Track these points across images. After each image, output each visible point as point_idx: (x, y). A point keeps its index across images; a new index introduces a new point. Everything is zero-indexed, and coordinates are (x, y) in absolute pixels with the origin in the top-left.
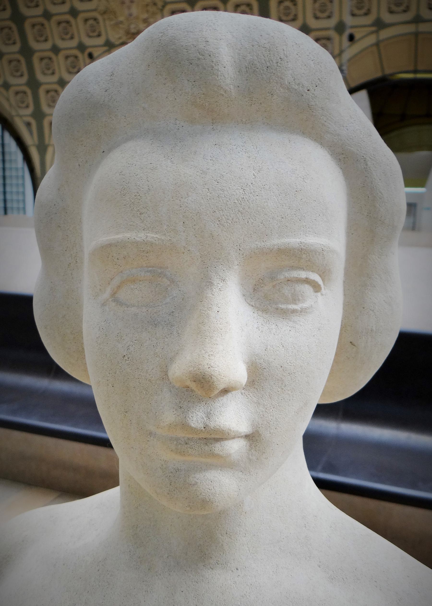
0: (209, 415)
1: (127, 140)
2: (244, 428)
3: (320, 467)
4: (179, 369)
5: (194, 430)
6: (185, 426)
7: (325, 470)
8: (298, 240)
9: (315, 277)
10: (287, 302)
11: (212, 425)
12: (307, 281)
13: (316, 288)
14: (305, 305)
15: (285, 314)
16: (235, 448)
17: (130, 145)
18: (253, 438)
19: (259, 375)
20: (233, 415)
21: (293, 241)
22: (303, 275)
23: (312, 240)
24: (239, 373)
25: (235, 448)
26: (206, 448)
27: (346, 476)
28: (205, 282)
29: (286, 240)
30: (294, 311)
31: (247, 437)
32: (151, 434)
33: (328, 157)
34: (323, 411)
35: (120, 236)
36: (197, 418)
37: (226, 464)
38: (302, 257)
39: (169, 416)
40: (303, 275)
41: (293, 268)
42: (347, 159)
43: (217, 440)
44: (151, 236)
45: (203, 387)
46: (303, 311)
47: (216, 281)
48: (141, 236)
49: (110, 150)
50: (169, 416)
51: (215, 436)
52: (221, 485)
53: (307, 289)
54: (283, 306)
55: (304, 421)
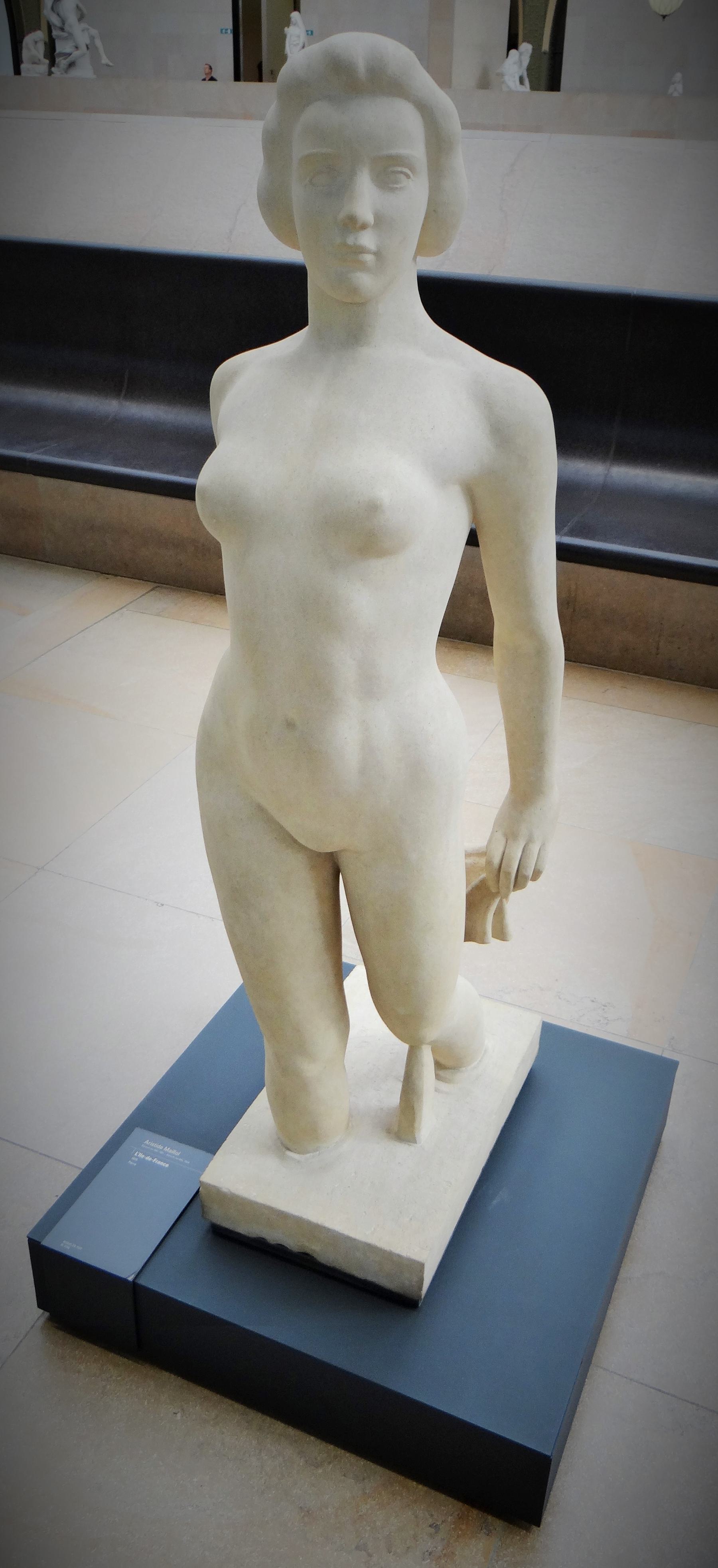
0: (356, 239)
3: (566, 529)
4: (342, 215)
6: (345, 244)
7: (571, 533)
12: (401, 172)
13: (408, 176)
15: (392, 190)
18: (378, 254)
19: (380, 219)
21: (394, 152)
22: (399, 169)
23: (403, 151)
24: (370, 218)
25: (369, 258)
27: (605, 541)
28: (353, 174)
36: (350, 241)
37: (363, 267)
38: (398, 160)
40: (399, 169)
43: (361, 253)
45: (352, 224)
51: (360, 250)
52: (365, 281)
53: (402, 177)
54: (391, 186)
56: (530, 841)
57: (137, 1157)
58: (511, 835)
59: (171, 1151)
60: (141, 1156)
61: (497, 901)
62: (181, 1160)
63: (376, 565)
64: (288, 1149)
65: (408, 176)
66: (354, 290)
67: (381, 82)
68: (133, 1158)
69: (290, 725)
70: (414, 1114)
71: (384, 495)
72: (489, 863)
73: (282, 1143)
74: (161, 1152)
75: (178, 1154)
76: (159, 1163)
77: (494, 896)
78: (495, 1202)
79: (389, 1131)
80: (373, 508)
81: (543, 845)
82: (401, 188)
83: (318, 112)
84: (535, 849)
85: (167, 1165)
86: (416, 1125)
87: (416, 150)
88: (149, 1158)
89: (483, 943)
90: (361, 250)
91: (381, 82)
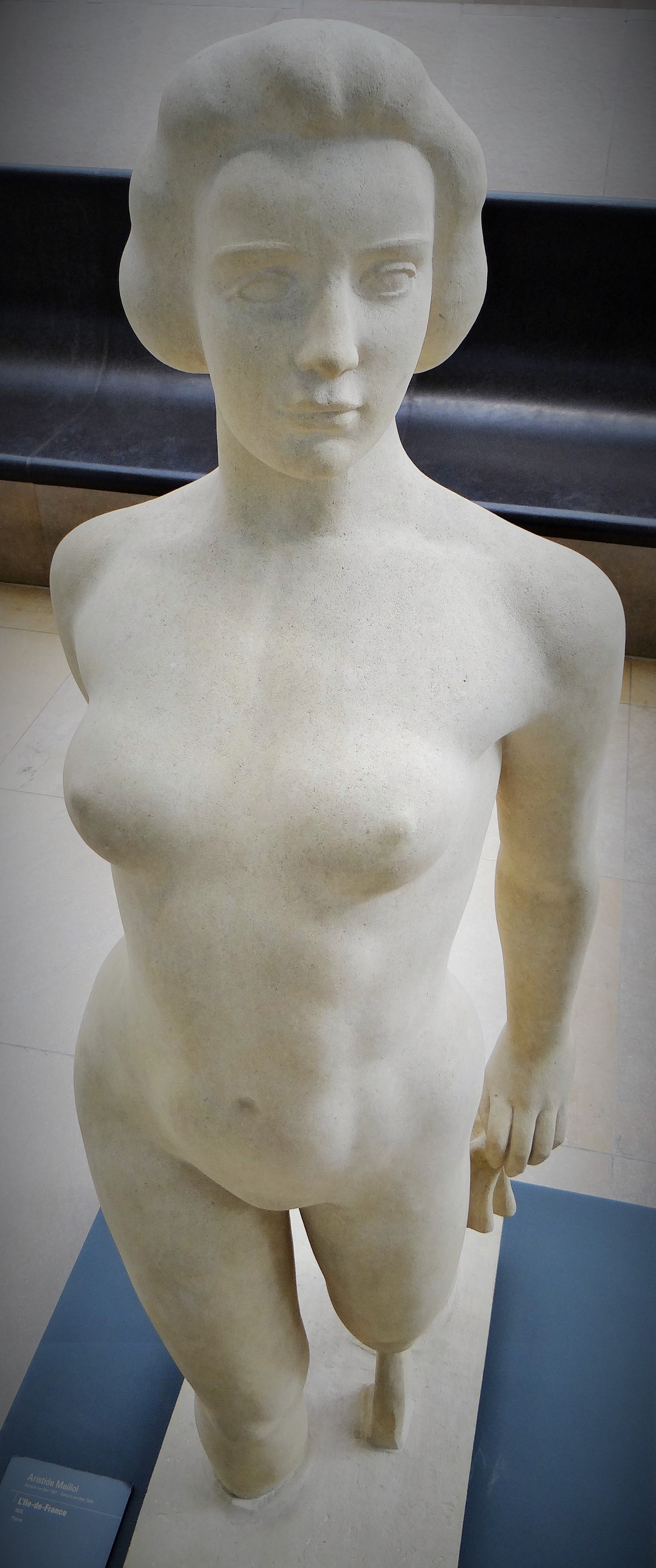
0: (331, 393)
1: (246, 149)
2: (357, 402)
4: (308, 355)
5: (320, 406)
6: (313, 403)
8: (397, 239)
9: (410, 266)
10: (388, 290)
11: (334, 400)
12: (404, 271)
13: (411, 274)
14: (402, 291)
15: (385, 300)
16: (350, 418)
17: (249, 155)
18: (363, 410)
19: (368, 356)
20: (348, 391)
21: (392, 240)
22: (400, 266)
23: (408, 237)
26: (329, 421)
28: (322, 282)
29: (387, 240)
30: (393, 297)
31: (358, 409)
32: (279, 412)
33: (419, 153)
34: (423, 382)
35: (251, 244)
36: (321, 396)
37: (341, 433)
39: (298, 396)
40: (400, 266)
41: (392, 261)
43: (337, 413)
44: (279, 244)
45: (330, 369)
46: (401, 296)
47: (332, 279)
48: (270, 244)
49: (229, 157)
50: (298, 396)
52: (337, 450)
53: (404, 276)
54: (384, 294)
55: (395, 395)
56: (545, 1108)
57: (21, 1507)
58: (518, 1103)
59: (65, 1487)
60: (27, 1503)
61: (497, 1176)
62: (81, 1499)
63: (386, 901)
64: (234, 1496)
65: (411, 274)
66: (325, 469)
67: (374, 115)
68: (18, 1511)
69: (245, 1106)
70: (393, 1420)
71: (407, 814)
72: (495, 1146)
73: (224, 1488)
74: (53, 1492)
75: (77, 1490)
76: (54, 1511)
77: (493, 1172)
78: (493, 1481)
79: (357, 1434)
80: (393, 838)
81: (562, 1108)
82: (401, 296)
83: (250, 172)
84: (552, 1117)
85: (65, 1513)
86: (397, 1431)
88: (38, 1506)
89: (484, 1231)
90: (337, 409)
91: (374, 115)
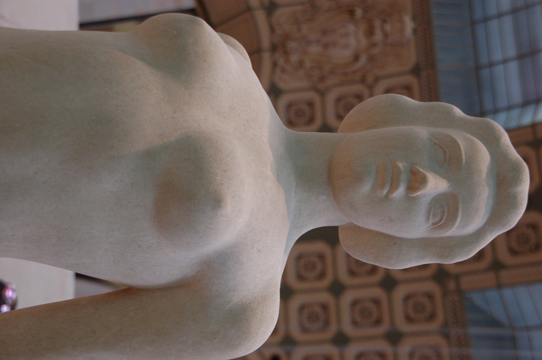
15: (429, 211)
28: (449, 180)
30: (429, 215)
40: (445, 218)
42: (479, 234)
53: (437, 220)
54: (432, 211)
87: (454, 231)
90: (394, 187)
